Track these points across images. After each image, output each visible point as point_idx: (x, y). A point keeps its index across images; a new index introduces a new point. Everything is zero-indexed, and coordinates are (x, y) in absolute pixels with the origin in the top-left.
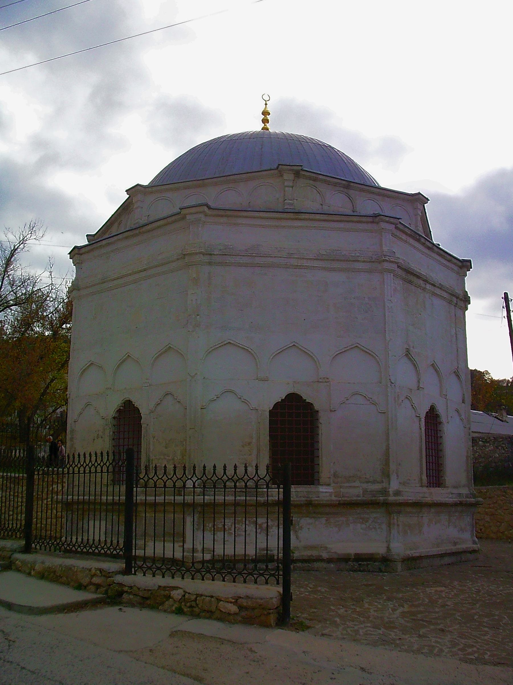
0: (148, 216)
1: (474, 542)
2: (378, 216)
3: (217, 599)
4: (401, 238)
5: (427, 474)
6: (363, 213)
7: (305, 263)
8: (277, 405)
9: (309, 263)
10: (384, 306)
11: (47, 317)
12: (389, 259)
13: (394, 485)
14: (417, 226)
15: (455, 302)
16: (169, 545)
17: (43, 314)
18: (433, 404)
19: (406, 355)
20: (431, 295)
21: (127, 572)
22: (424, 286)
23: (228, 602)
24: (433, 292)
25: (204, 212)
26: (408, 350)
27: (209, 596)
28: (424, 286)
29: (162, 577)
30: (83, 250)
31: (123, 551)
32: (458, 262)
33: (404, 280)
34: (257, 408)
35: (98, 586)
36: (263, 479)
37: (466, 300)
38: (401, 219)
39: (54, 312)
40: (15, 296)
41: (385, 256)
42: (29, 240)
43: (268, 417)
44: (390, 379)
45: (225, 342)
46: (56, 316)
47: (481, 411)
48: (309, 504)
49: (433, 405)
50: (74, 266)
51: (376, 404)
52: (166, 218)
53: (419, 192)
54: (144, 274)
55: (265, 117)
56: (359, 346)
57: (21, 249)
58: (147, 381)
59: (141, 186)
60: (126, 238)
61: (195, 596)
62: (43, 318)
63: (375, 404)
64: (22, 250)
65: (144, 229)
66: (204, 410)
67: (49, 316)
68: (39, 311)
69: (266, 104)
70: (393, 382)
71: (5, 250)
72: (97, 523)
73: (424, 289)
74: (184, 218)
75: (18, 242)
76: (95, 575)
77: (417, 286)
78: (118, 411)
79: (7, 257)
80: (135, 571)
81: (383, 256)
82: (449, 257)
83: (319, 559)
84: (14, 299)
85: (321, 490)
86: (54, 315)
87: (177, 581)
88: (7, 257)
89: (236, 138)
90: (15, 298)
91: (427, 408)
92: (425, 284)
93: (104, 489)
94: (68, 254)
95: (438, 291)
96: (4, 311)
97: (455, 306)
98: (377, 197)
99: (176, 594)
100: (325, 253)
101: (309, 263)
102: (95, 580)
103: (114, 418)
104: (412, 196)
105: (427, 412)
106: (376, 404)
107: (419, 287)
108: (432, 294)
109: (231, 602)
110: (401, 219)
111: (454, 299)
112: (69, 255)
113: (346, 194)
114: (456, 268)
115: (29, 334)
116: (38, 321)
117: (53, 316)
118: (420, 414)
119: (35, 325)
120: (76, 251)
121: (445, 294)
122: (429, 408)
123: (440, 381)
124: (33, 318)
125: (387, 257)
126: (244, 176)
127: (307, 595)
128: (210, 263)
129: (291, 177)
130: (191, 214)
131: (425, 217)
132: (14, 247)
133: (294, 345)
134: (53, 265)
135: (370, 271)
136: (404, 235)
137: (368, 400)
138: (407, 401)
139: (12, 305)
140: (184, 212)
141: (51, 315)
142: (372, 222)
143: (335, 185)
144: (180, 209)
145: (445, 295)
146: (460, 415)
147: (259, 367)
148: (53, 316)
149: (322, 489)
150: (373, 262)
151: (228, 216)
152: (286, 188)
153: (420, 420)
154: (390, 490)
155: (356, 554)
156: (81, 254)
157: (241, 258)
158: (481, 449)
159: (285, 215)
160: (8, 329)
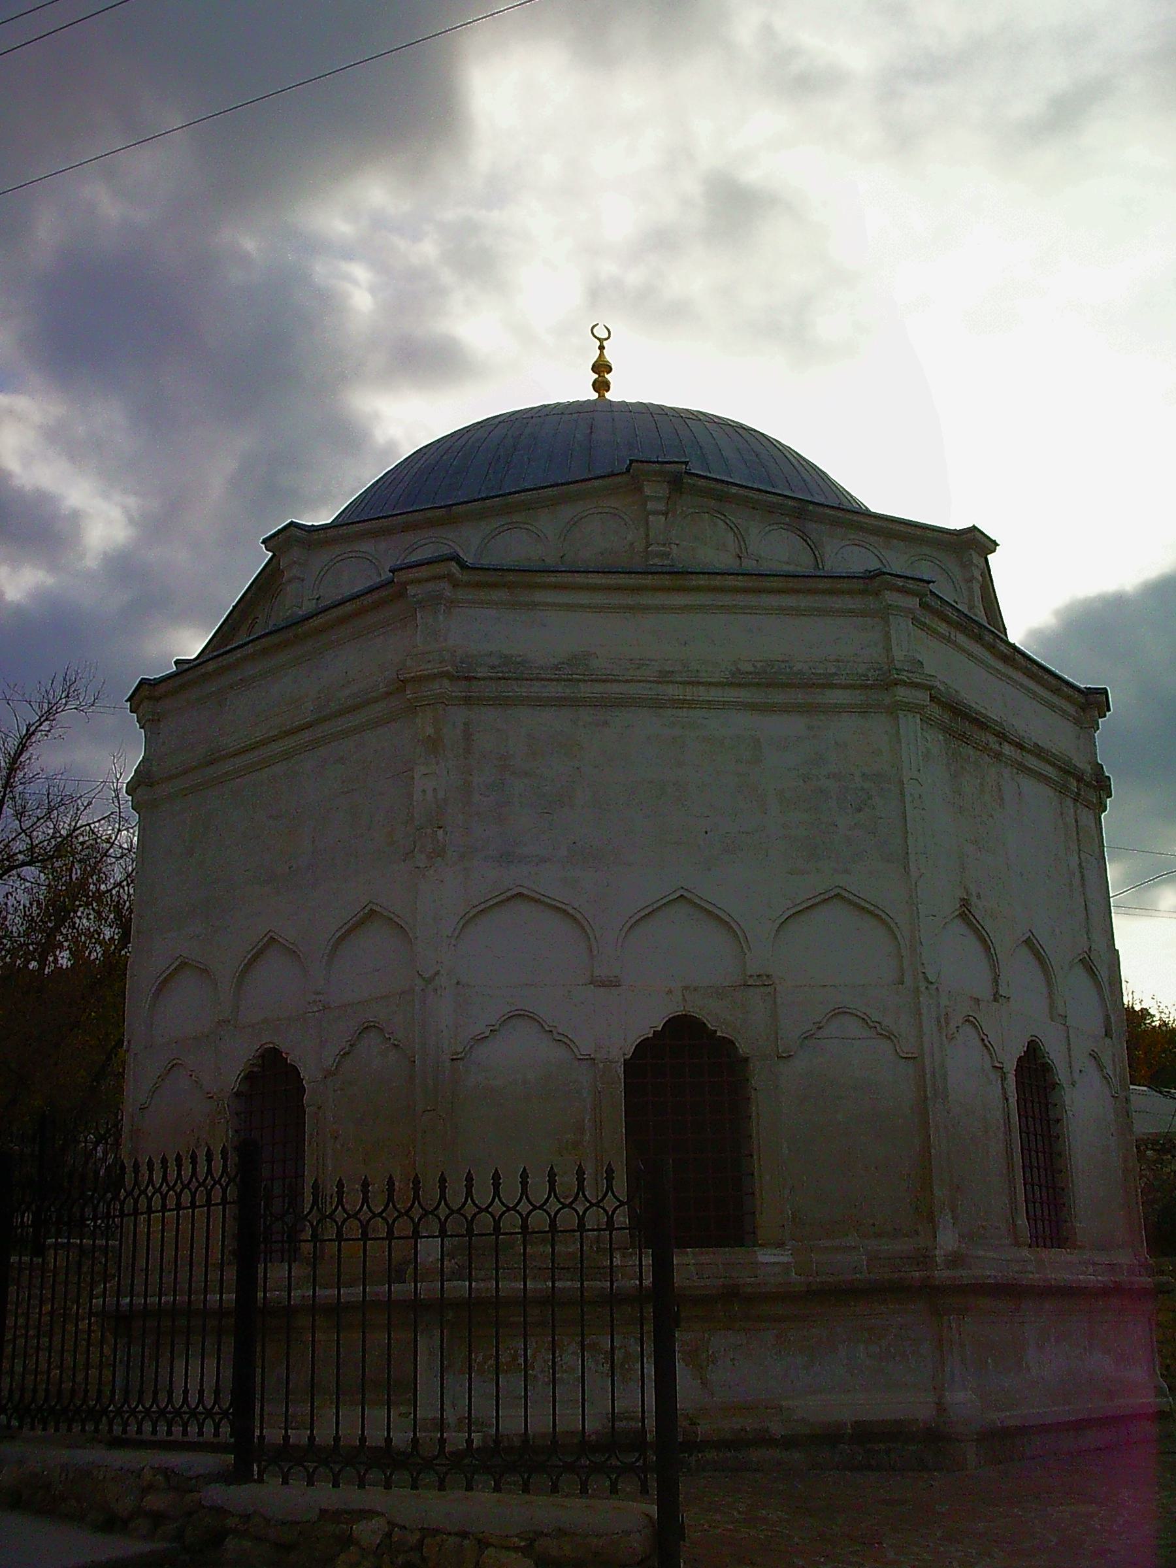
0: (317, 599)
1: (1159, 1392)
2: (878, 575)
3: (479, 1541)
4: (935, 631)
5: (1027, 1212)
6: (841, 570)
7: (703, 693)
8: (643, 1047)
9: (714, 694)
10: (902, 794)
11: (108, 894)
12: (908, 678)
13: (947, 1240)
14: (971, 608)
15: (1076, 790)
16: (377, 1414)
17: (98, 890)
18: (1034, 1038)
19: (962, 916)
20: (1015, 770)
21: (239, 1475)
22: (997, 747)
23: (507, 1548)
24: (1020, 764)
25: (449, 577)
26: (965, 903)
27: (456, 1534)
28: (997, 747)
29: (333, 1486)
30: (162, 688)
31: (231, 1417)
32: (1076, 695)
33: (946, 730)
34: (592, 1056)
35: (158, 1518)
36: (540, 1208)
37: (1102, 786)
38: (934, 582)
39: (125, 883)
40: (29, 842)
41: (899, 671)
42: (62, 711)
43: (622, 1076)
44: (924, 973)
45: (509, 894)
46: (128, 890)
47: (1145, 1086)
48: (731, 1294)
49: (1032, 1041)
50: (140, 728)
51: (892, 1037)
52: (358, 597)
53: (974, 526)
54: (306, 736)
55: (599, 376)
56: (844, 893)
57: (43, 733)
58: (318, 998)
59: (299, 528)
60: (265, 652)
61: (417, 1536)
62: (99, 896)
63: (889, 1036)
64: (46, 735)
65: (307, 626)
66: (460, 1063)
67: (114, 892)
68: (90, 881)
69: (602, 348)
70: (933, 981)
71: (7, 736)
72: (195, 1364)
73: (998, 756)
74: (401, 594)
75: (38, 718)
76: (150, 1488)
77: (980, 748)
78: (246, 1078)
79: (12, 754)
80: (260, 1474)
81: (894, 672)
82: (1054, 681)
83: (764, 1440)
84: (28, 849)
85: (763, 1258)
86: (124, 890)
87: (373, 1497)
88: (12, 754)
89: (529, 415)
90: (28, 846)
91: (1019, 1050)
92: (1001, 744)
93: (214, 1275)
94: (126, 701)
95: (1032, 762)
96: (4, 878)
97: (1075, 799)
98: (872, 539)
99: (368, 1532)
100: (751, 669)
101: (714, 694)
102: (155, 1502)
103: (237, 1095)
104: (956, 535)
105: (1020, 1059)
106: (892, 1037)
107: (986, 749)
108: (1018, 769)
109: (516, 1549)
110: (934, 582)
111: (1073, 784)
112: (129, 703)
113: (798, 533)
114: (1070, 709)
115: (67, 934)
116: (88, 904)
117: (121, 890)
118: (1002, 1063)
119: (79, 914)
120: (145, 692)
121: (1050, 769)
122: (1024, 1047)
123: (1049, 983)
124: (75, 898)
125: (905, 673)
126: (550, 492)
127: (730, 1530)
128: (468, 701)
129: (662, 490)
130: (419, 581)
131: (991, 590)
132: (28, 730)
133: (682, 895)
134: (121, 774)
135: (864, 711)
136: (944, 625)
137: (871, 1028)
138: (968, 1029)
139: (24, 864)
140: (403, 576)
141: (117, 889)
142: (863, 592)
143: (771, 509)
144: (390, 571)
145: (1050, 771)
146: (1101, 1067)
147: (595, 953)
148: (121, 890)
149: (766, 1256)
150: (871, 687)
151: (510, 586)
152: (651, 518)
153: (1004, 1078)
154: (937, 1252)
155: (856, 1423)
156: (158, 699)
157: (545, 686)
158: (1153, 1169)
159: (649, 581)
160: (15, 923)
